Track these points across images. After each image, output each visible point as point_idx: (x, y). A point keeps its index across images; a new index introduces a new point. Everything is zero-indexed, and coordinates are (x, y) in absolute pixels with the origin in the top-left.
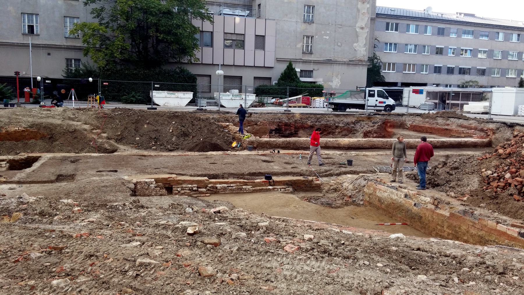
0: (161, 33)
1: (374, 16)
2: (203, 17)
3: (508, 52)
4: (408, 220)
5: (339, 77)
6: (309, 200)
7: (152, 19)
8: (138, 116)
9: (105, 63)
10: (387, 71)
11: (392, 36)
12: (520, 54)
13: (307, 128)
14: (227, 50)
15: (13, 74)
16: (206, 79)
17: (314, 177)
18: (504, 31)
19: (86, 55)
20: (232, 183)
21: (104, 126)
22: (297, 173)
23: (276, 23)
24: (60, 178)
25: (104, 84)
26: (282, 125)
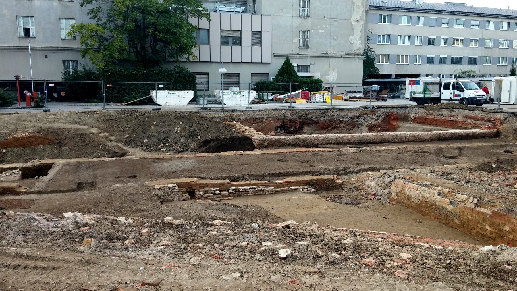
0: (159, 32)
1: (367, 9)
2: (200, 15)
3: (498, 40)
4: (444, 219)
5: (336, 71)
6: (332, 200)
7: (151, 19)
8: (145, 118)
9: (104, 64)
10: (380, 63)
11: (386, 28)
12: (510, 43)
13: (311, 124)
14: (223, 47)
15: (13, 79)
16: (205, 77)
17: (335, 176)
18: (494, 19)
19: (84, 56)
20: (253, 185)
21: (112, 129)
22: (317, 172)
23: (272, 18)
24: (80, 187)
25: (108, 85)
26: (287, 122)
